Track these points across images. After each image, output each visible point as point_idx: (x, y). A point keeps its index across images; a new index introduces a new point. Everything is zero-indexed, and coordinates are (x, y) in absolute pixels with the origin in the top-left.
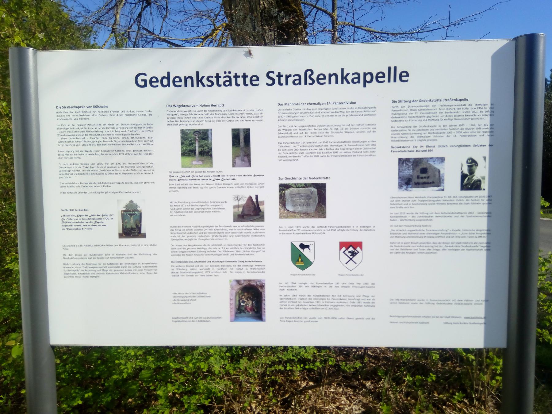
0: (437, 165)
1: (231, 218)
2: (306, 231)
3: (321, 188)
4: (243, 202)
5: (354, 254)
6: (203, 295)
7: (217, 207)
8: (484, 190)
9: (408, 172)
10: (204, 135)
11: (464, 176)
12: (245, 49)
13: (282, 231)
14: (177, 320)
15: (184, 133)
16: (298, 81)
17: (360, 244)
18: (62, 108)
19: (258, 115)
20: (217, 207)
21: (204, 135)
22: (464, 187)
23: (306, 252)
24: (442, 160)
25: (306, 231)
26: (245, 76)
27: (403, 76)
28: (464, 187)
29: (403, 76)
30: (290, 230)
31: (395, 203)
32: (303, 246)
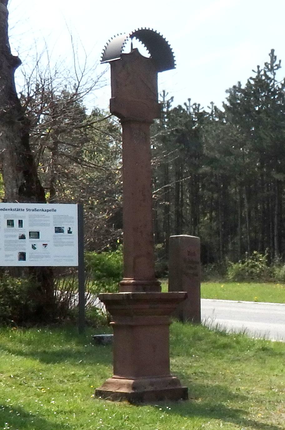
0: (63, 228)
1: (17, 258)
2: (34, 241)
3: (38, 233)
4: (21, 235)
5: (46, 246)
6: (12, 255)
7: (15, 236)
8: (69, 232)
9: (57, 230)
10: (12, 221)
11: (68, 231)
12: (28, 263)
13: (30, 241)
14: (6, 260)
15: (8, 220)
16: (33, 210)
17: (47, 244)
18: (26, 210)
19: (24, 217)
20: (15, 236)
21: (12, 221)
22: (68, 233)
23: (35, 246)
24: (63, 227)
25: (34, 241)
26: (21, 209)
27: (55, 211)
28: (68, 233)
29: (55, 211)
30: (32, 242)
31: (54, 236)
32: (35, 245)
